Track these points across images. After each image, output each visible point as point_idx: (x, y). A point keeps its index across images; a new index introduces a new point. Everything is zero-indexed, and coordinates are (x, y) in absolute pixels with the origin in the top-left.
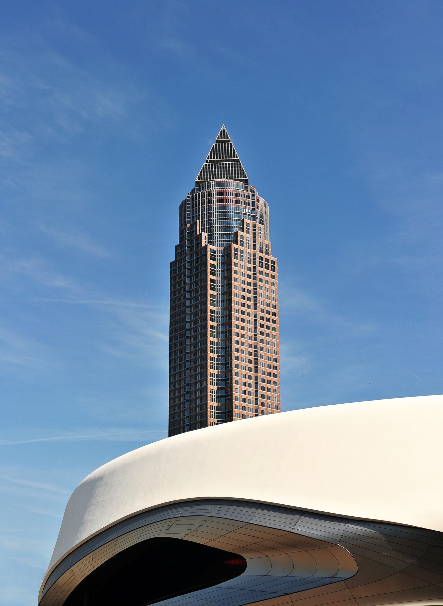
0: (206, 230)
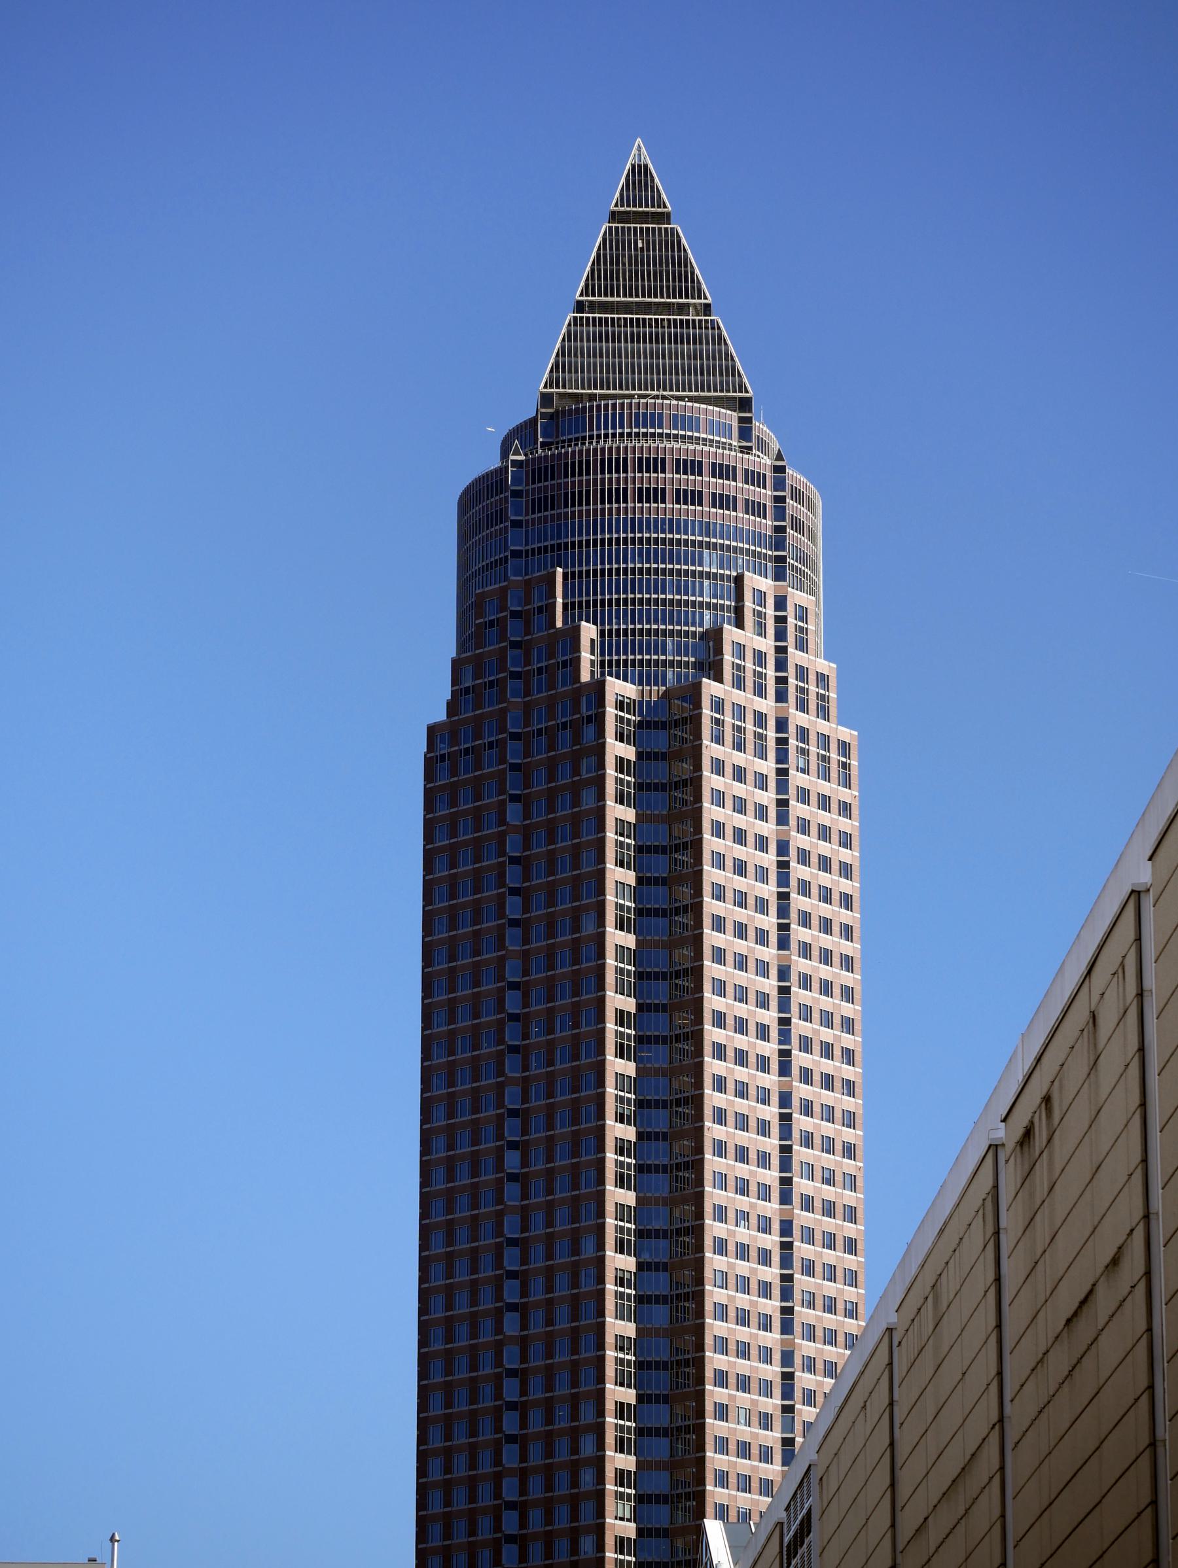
0: (595, 613)
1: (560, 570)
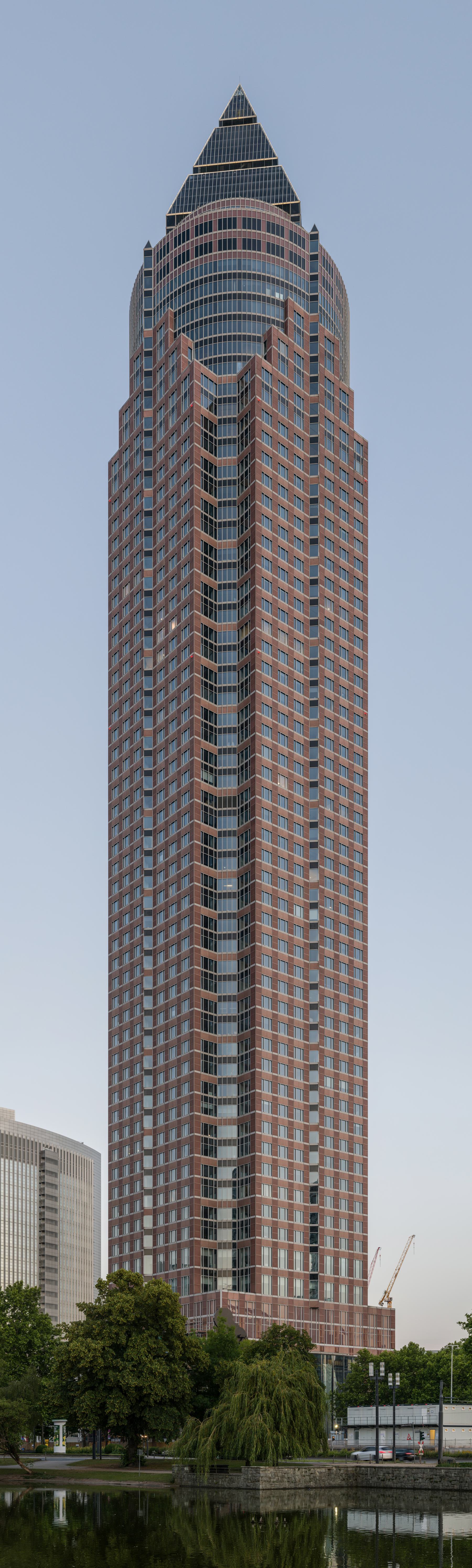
0: (192, 332)
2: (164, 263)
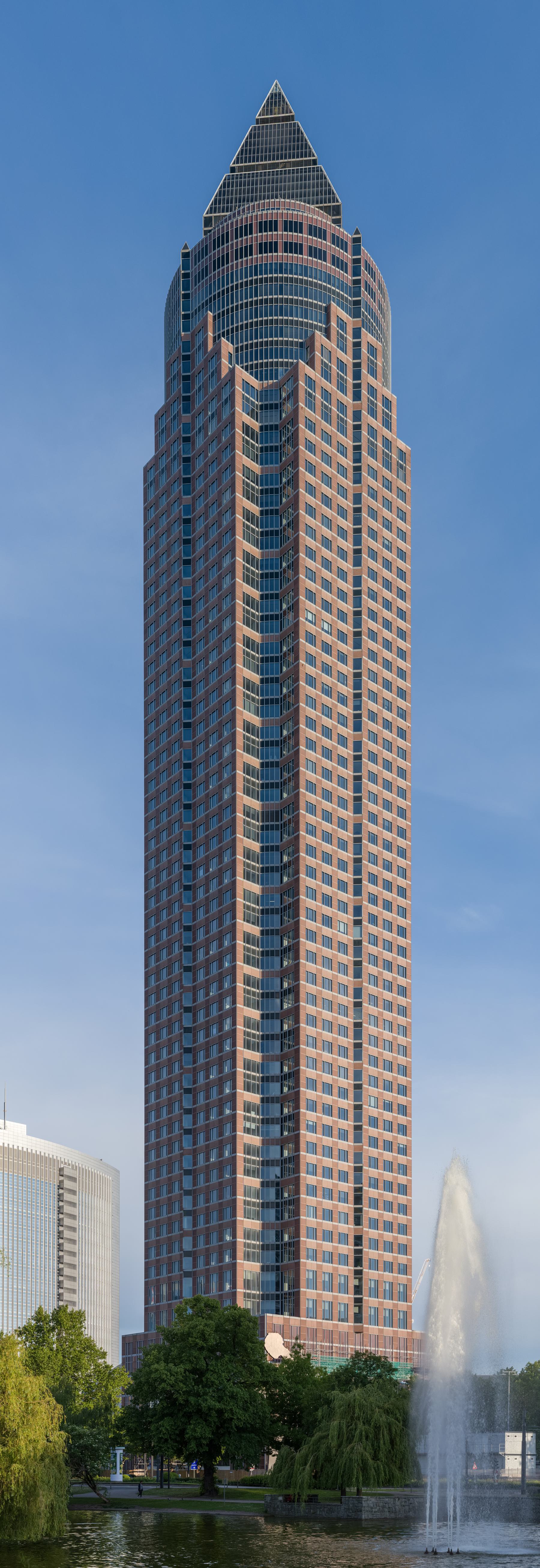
0: (232, 337)
1: (210, 314)
2: (202, 266)
